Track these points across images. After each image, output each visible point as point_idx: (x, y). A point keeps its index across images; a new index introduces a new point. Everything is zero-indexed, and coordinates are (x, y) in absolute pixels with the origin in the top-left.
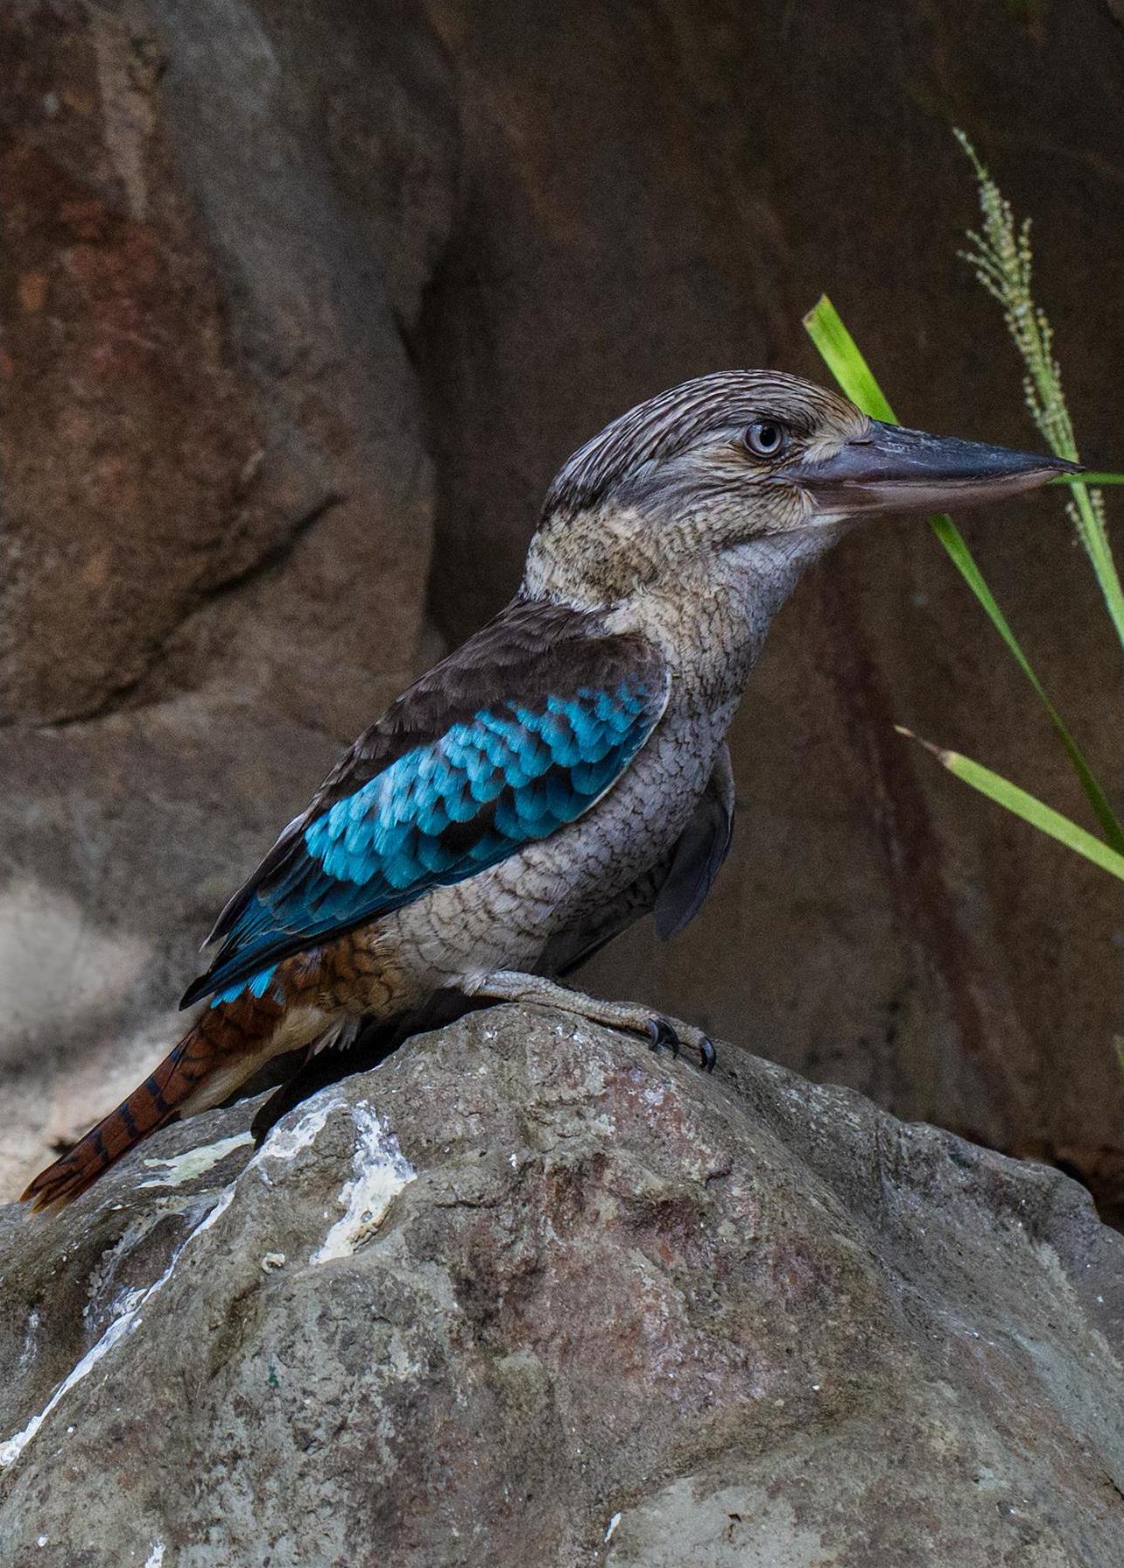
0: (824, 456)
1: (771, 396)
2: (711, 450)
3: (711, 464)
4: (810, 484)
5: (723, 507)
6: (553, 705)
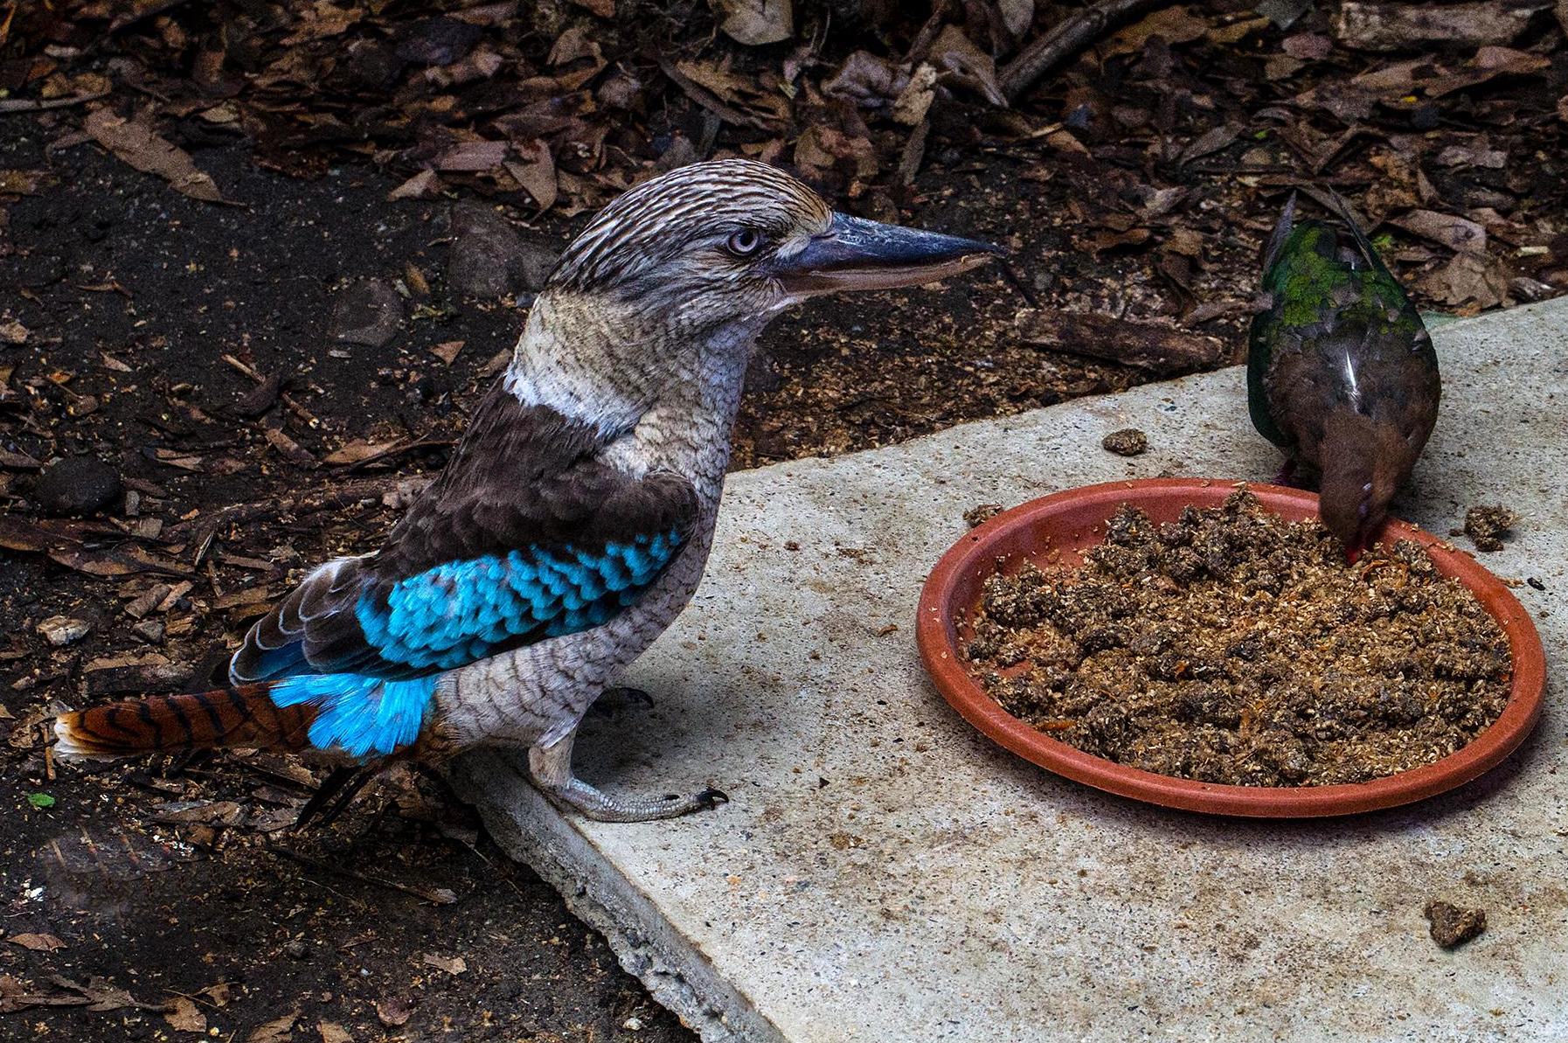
0: (795, 251)
1: (753, 207)
2: (700, 254)
3: (700, 265)
4: (779, 275)
5: (706, 303)
6: (611, 550)
